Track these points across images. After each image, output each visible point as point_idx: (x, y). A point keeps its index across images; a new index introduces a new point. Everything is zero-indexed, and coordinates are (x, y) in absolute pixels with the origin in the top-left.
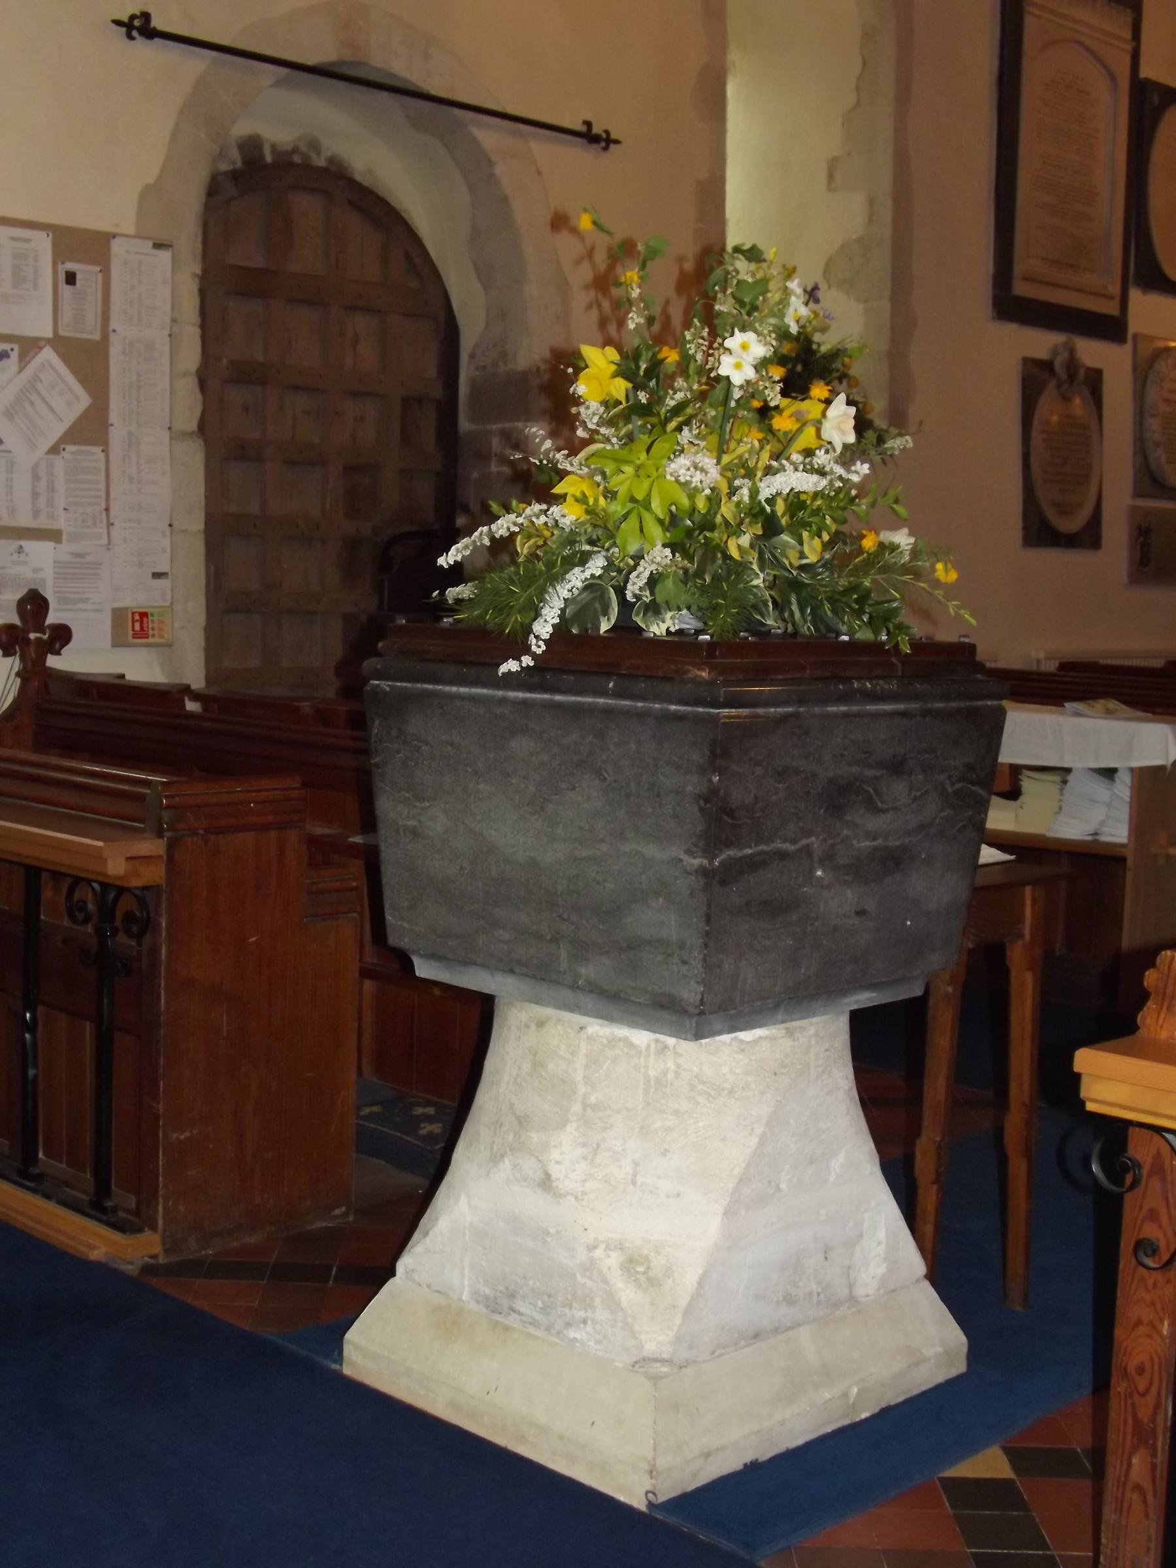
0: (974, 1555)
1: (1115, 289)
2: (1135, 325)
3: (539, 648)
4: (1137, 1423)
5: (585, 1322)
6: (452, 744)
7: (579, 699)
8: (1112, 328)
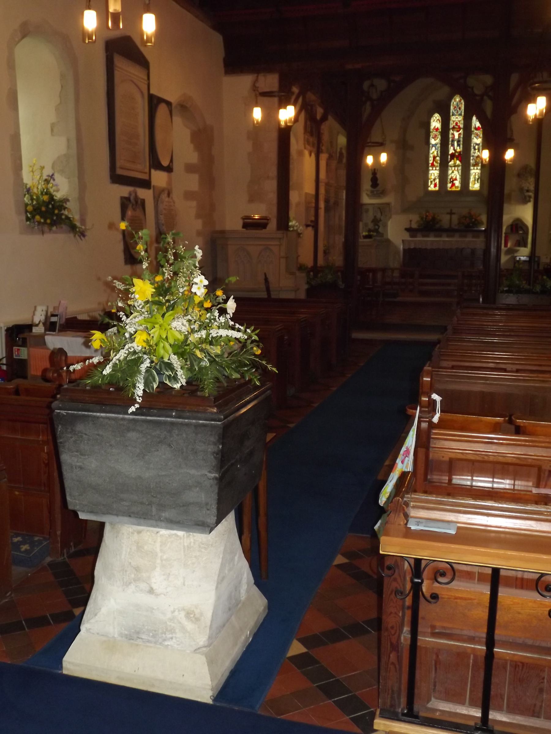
0: (317, 686)
1: (147, 170)
2: (154, 182)
3: (139, 400)
4: (392, 644)
5: (172, 638)
6: (98, 435)
7: (158, 418)
8: (146, 184)
